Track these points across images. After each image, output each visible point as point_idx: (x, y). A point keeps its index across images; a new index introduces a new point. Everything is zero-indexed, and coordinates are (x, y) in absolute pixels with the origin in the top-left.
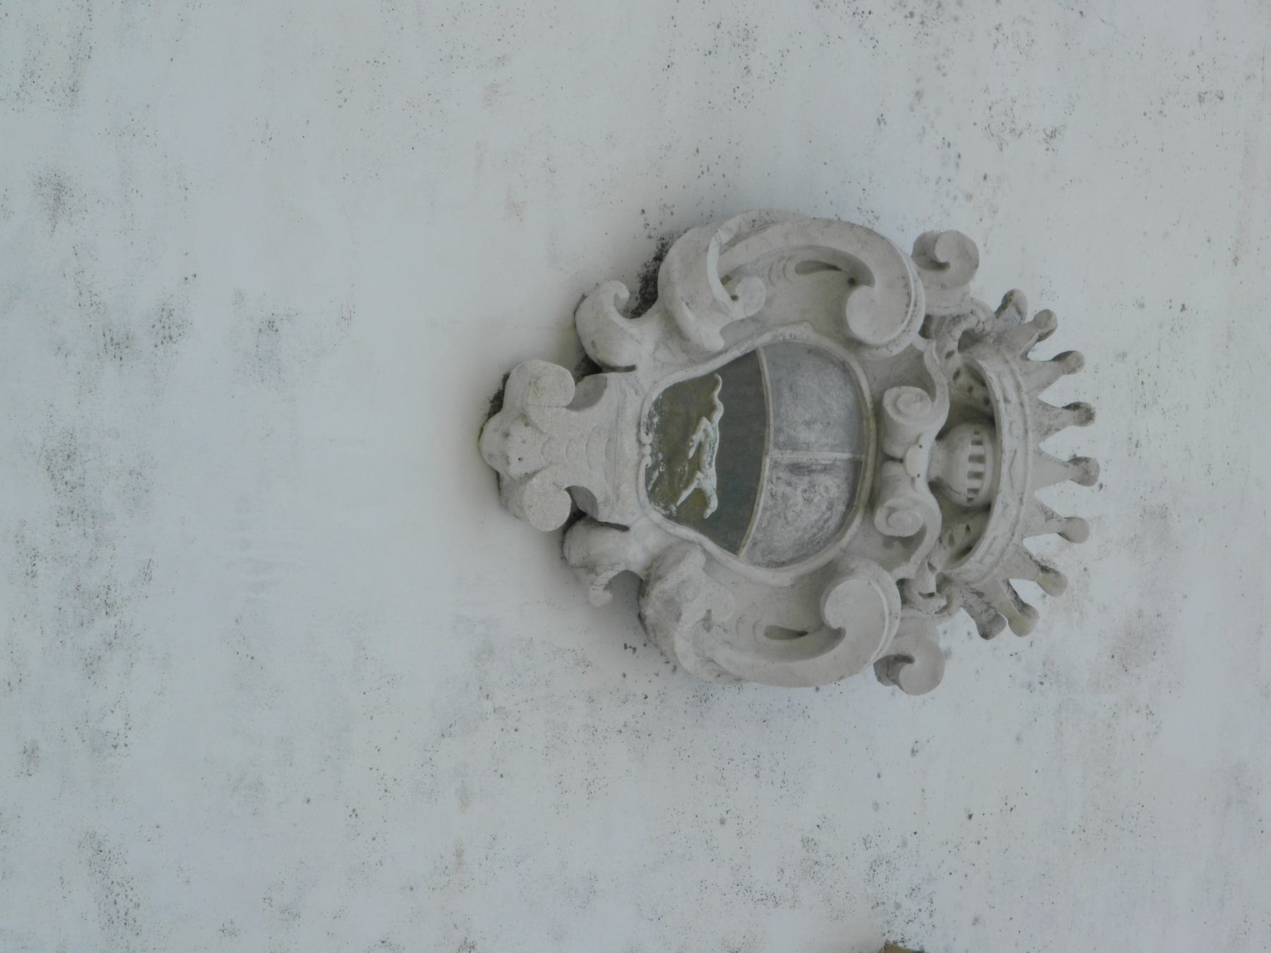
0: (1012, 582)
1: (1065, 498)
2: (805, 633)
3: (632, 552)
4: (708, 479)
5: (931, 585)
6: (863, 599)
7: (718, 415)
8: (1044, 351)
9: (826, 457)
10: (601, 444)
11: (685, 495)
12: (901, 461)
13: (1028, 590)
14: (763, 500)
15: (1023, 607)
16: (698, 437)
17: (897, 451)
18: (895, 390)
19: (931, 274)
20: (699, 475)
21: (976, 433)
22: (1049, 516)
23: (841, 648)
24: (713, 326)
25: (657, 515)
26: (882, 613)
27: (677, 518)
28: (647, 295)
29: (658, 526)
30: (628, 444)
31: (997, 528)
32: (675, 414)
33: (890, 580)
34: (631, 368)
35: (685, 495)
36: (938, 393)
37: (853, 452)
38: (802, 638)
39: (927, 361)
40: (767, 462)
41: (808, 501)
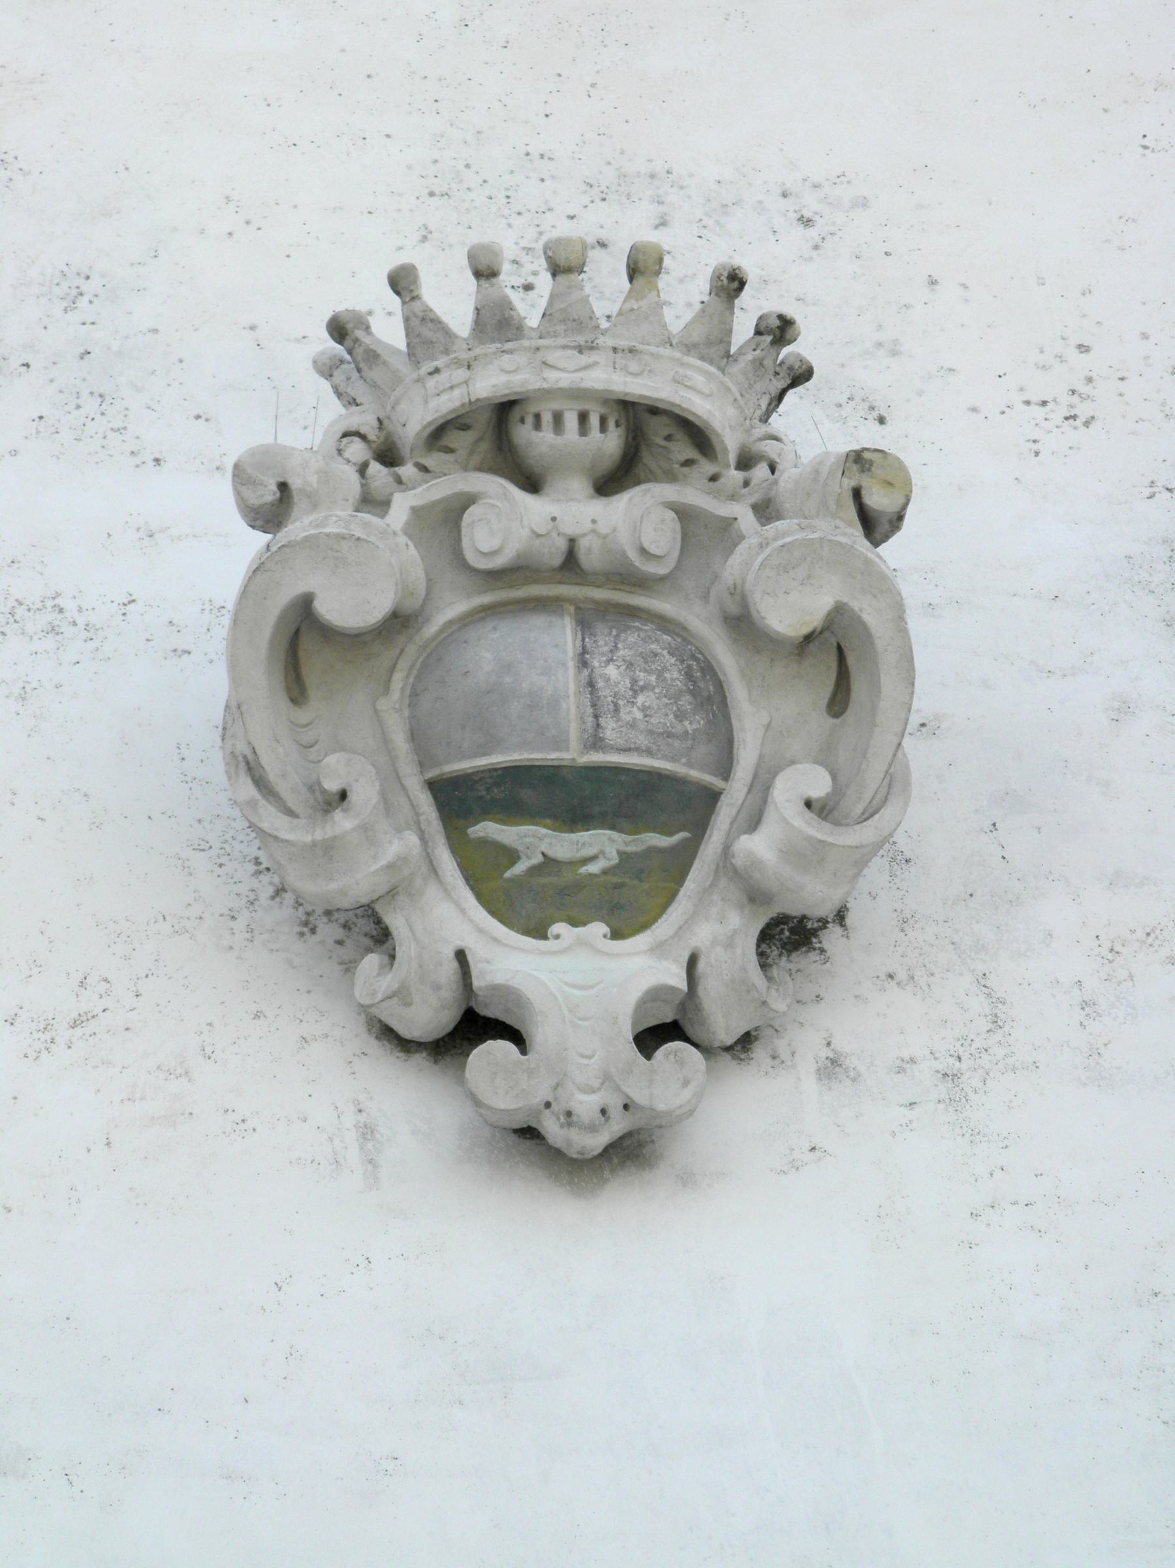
2: (840, 661)
10: (579, 984)
12: (572, 541)
21: (522, 421)
24: (390, 842)
37: (562, 616)
38: (845, 650)
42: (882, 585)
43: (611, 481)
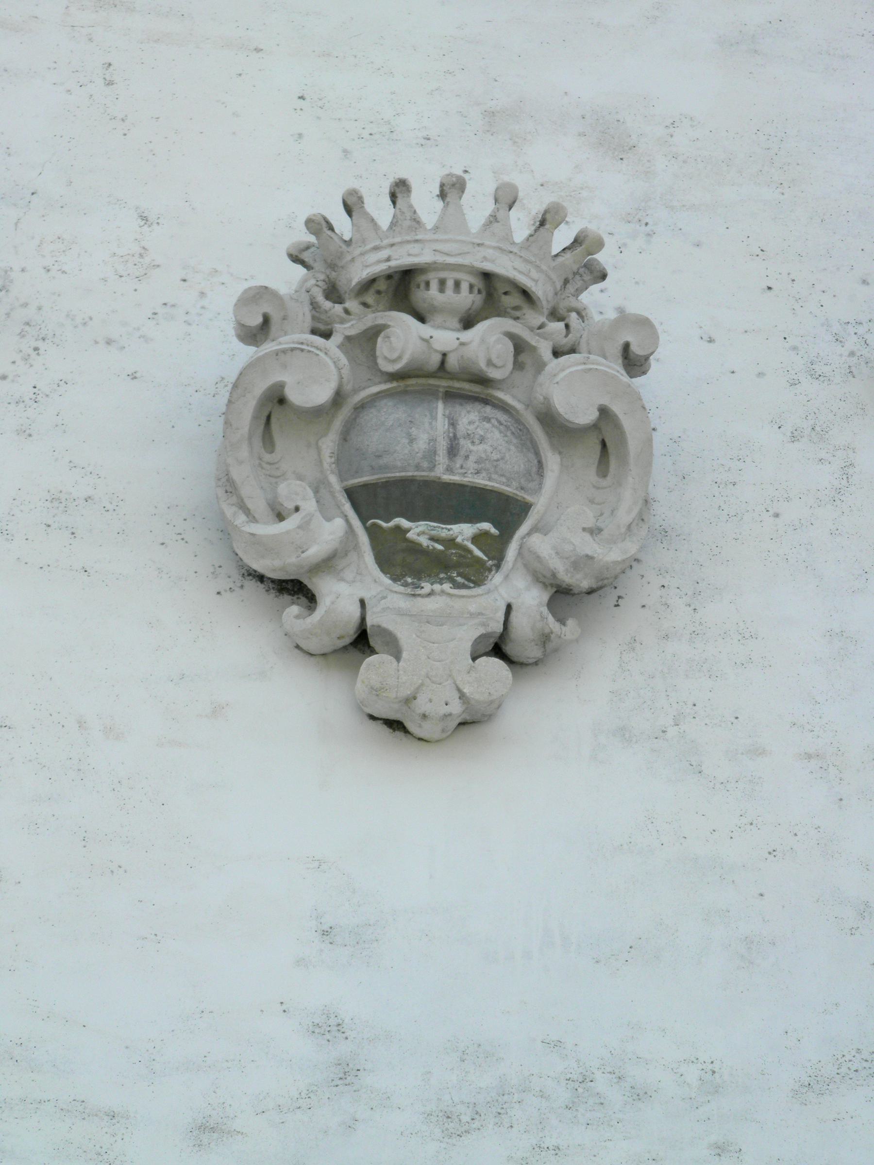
1: (477, 206)
3: (531, 601)
6: (572, 389)
7: (404, 523)
8: (343, 225)
9: (441, 425)
10: (434, 633)
11: (478, 553)
13: (562, 238)
14: (481, 481)
15: (577, 242)
16: (424, 541)
17: (436, 359)
18: (380, 361)
19: (274, 328)
22: (493, 219)
23: (617, 408)
25: (497, 578)
28: (295, 589)
29: (507, 577)
31: (504, 267)
32: (401, 561)
33: (554, 364)
34: (362, 603)
35: (478, 553)
36: (380, 321)
39: (352, 332)
40: (447, 478)
41: (482, 440)
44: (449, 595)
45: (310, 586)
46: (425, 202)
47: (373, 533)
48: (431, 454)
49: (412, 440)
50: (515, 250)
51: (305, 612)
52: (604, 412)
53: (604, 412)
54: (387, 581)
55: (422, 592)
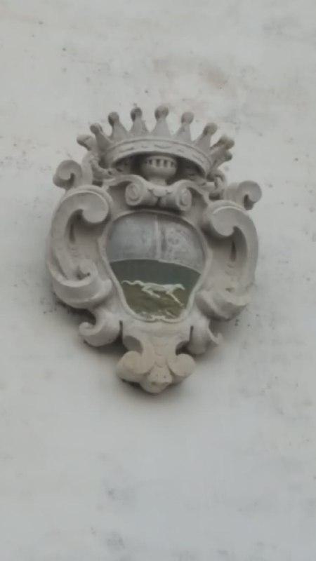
0: (211, 145)
1: (173, 122)
2: (234, 245)
3: (202, 324)
4: (169, 288)
5: (211, 184)
6: (221, 218)
7: (141, 283)
8: (107, 130)
9: (158, 233)
10: (156, 339)
11: (176, 300)
13: (214, 139)
14: (177, 262)
15: (221, 142)
16: (151, 293)
17: (155, 200)
18: (127, 200)
19: (76, 181)
20: (168, 293)
22: (182, 130)
23: (242, 228)
25: (185, 313)
26: (228, 209)
27: (185, 300)
28: (84, 314)
29: (190, 313)
30: (157, 326)
31: (189, 154)
32: (141, 303)
33: (211, 204)
34: (121, 323)
35: (176, 300)
36: (127, 180)
39: (114, 184)
40: (161, 260)
41: (177, 241)
42: (249, 222)
43: (170, 180)
44: (165, 322)
45: (93, 313)
46: (149, 121)
47: (125, 287)
48: (154, 248)
49: (144, 241)
50: (192, 146)
51: (91, 326)
52: (236, 230)
53: (236, 230)
54: (133, 312)
55: (151, 320)
